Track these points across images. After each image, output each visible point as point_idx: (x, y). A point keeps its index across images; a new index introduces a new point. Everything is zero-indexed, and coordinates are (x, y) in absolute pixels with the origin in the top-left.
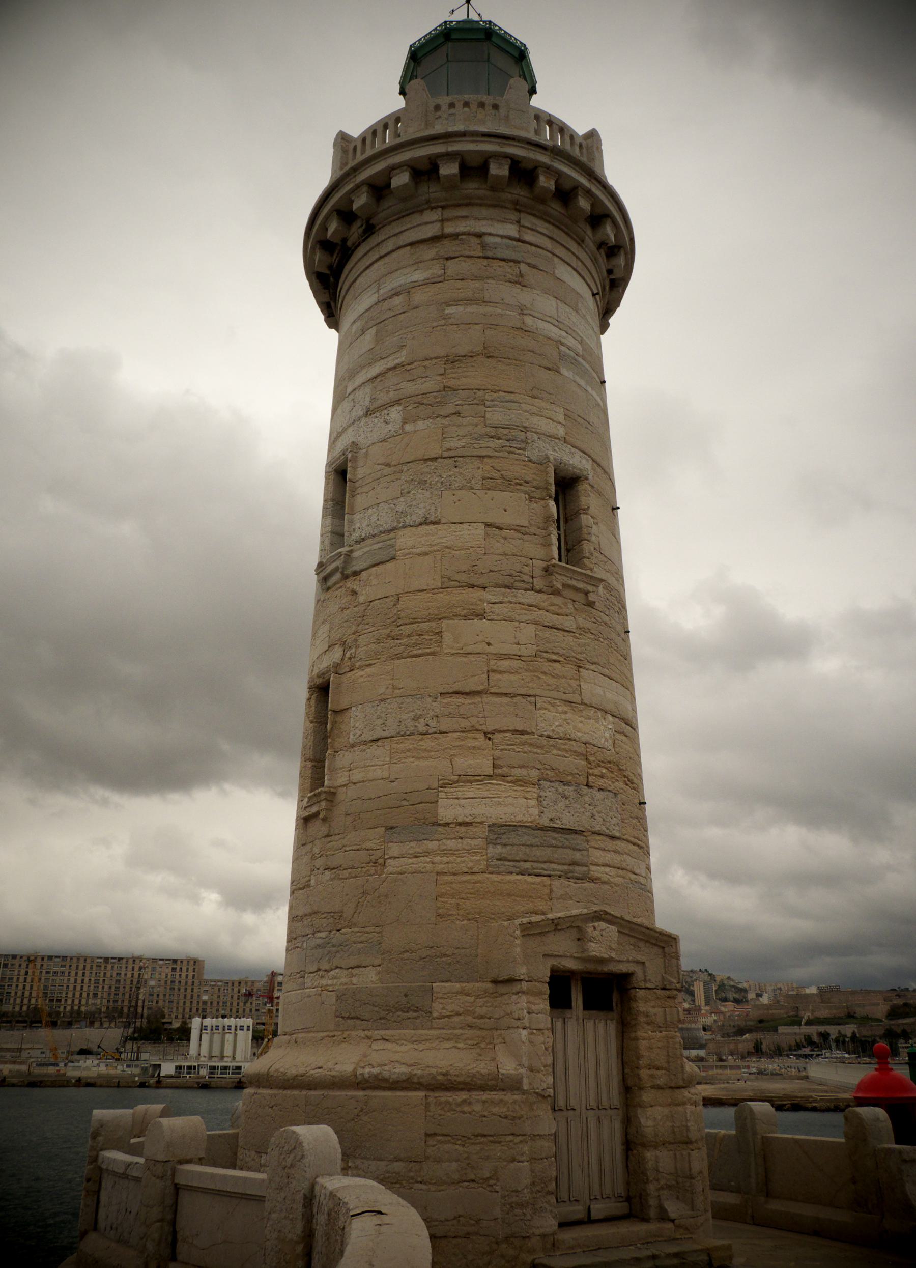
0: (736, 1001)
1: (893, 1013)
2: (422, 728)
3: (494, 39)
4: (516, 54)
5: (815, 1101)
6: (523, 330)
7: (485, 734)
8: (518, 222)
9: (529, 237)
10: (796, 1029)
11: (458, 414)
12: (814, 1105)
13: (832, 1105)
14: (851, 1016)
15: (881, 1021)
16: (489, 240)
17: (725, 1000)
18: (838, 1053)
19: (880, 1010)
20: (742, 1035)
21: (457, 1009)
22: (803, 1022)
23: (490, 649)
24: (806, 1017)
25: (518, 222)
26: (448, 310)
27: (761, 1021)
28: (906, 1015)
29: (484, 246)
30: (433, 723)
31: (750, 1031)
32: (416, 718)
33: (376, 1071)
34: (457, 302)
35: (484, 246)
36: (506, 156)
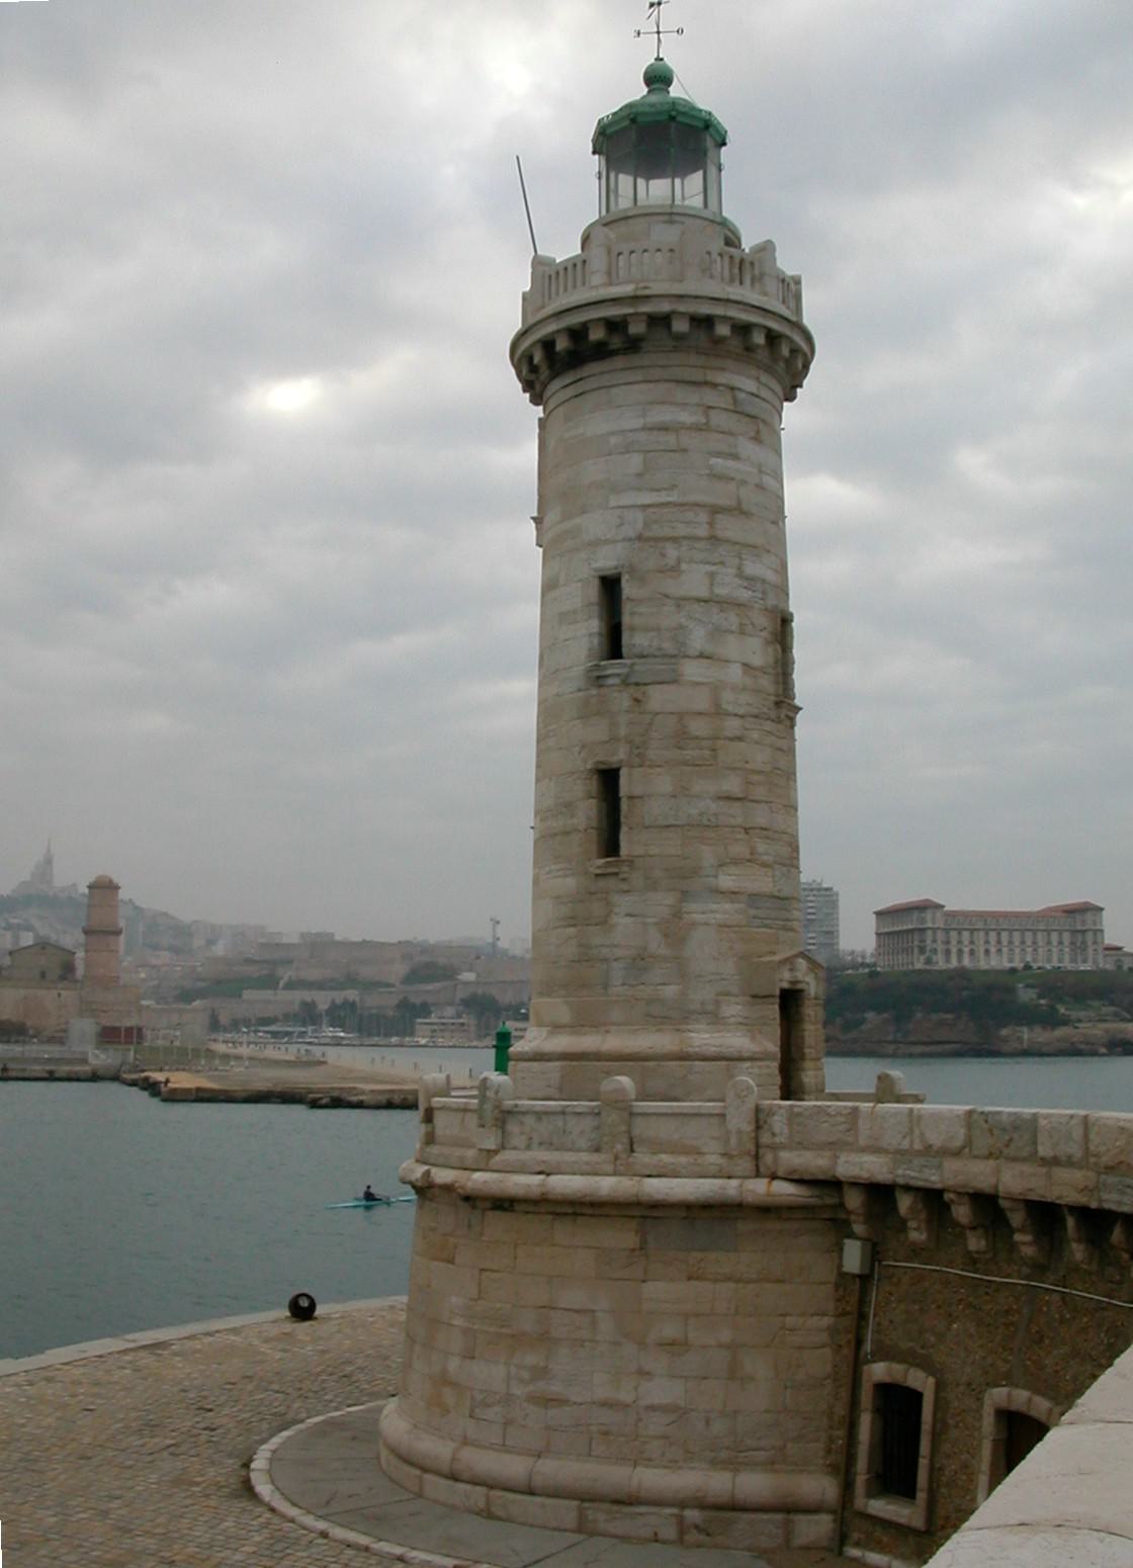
0: (176, 950)
1: (415, 976)
2: (705, 822)
3: (711, 130)
4: (720, 141)
5: (363, 1092)
6: (760, 487)
7: (745, 829)
8: (758, 378)
9: (764, 393)
10: (268, 994)
11: (722, 563)
12: (361, 1098)
13: (383, 1099)
14: (351, 981)
15: (393, 986)
16: (741, 396)
17: (156, 947)
18: (329, 1031)
19: (400, 970)
20: (190, 1002)
21: (734, 1013)
22: (282, 984)
23: (747, 766)
24: (286, 978)
25: (758, 378)
26: (713, 461)
27: (219, 982)
28: (431, 979)
29: (735, 401)
30: (713, 819)
31: (200, 994)
32: (701, 814)
33: (697, 1049)
34: (718, 454)
35: (735, 401)
36: (765, 327)
